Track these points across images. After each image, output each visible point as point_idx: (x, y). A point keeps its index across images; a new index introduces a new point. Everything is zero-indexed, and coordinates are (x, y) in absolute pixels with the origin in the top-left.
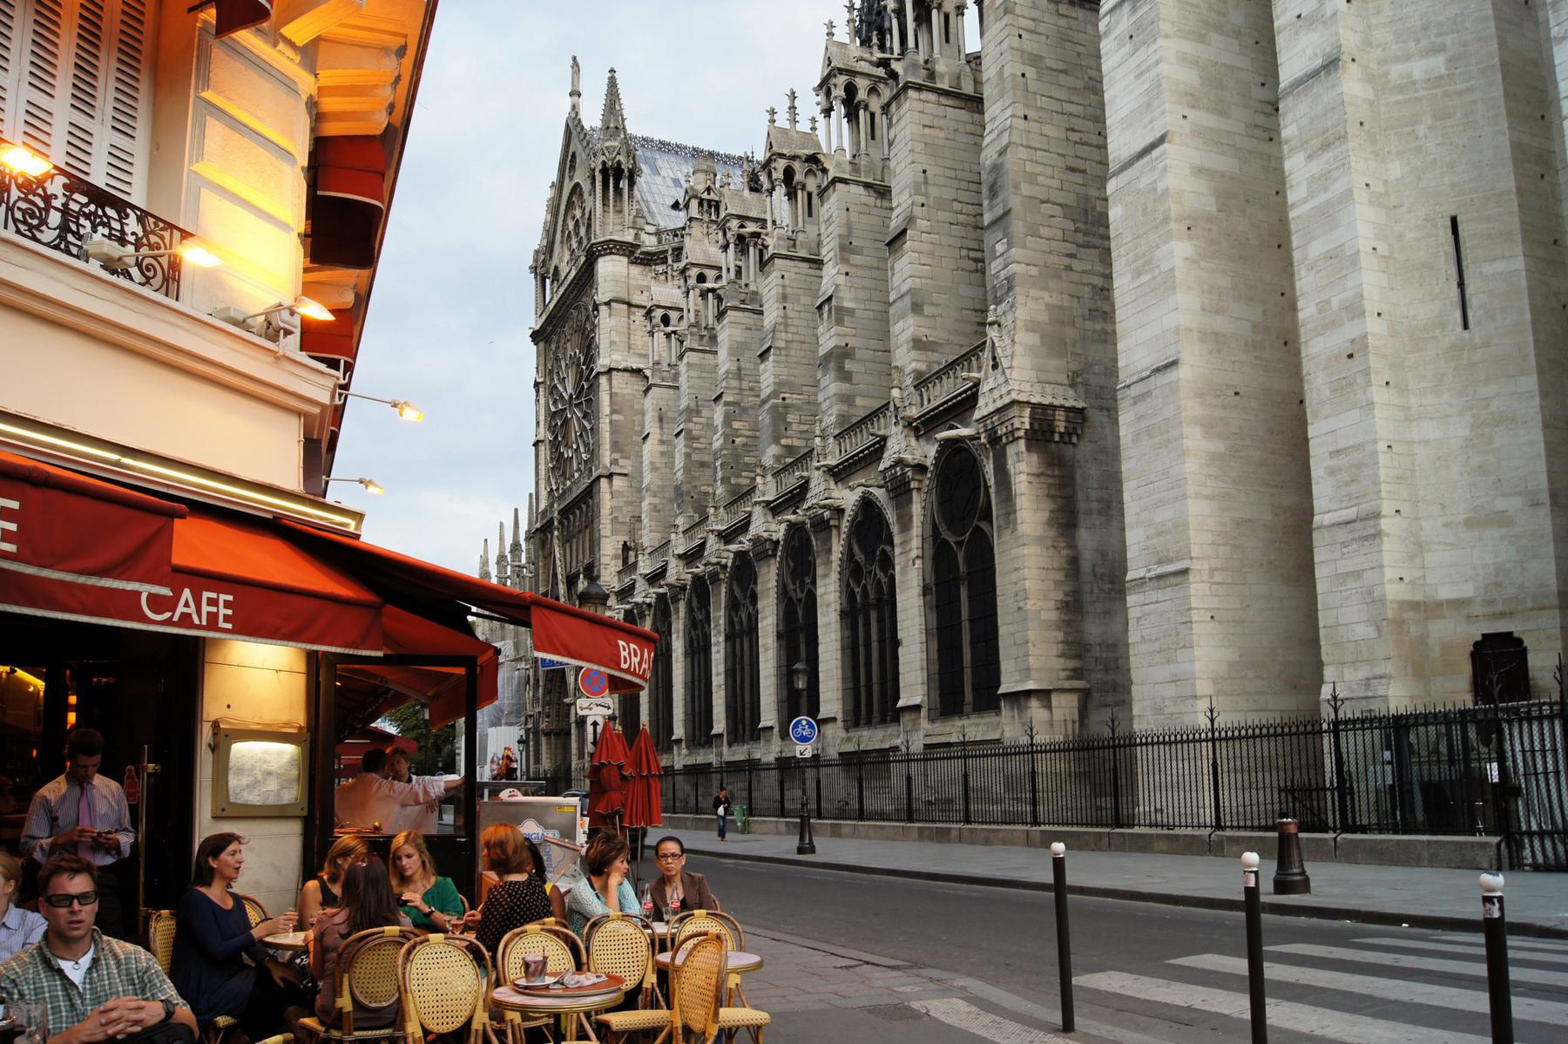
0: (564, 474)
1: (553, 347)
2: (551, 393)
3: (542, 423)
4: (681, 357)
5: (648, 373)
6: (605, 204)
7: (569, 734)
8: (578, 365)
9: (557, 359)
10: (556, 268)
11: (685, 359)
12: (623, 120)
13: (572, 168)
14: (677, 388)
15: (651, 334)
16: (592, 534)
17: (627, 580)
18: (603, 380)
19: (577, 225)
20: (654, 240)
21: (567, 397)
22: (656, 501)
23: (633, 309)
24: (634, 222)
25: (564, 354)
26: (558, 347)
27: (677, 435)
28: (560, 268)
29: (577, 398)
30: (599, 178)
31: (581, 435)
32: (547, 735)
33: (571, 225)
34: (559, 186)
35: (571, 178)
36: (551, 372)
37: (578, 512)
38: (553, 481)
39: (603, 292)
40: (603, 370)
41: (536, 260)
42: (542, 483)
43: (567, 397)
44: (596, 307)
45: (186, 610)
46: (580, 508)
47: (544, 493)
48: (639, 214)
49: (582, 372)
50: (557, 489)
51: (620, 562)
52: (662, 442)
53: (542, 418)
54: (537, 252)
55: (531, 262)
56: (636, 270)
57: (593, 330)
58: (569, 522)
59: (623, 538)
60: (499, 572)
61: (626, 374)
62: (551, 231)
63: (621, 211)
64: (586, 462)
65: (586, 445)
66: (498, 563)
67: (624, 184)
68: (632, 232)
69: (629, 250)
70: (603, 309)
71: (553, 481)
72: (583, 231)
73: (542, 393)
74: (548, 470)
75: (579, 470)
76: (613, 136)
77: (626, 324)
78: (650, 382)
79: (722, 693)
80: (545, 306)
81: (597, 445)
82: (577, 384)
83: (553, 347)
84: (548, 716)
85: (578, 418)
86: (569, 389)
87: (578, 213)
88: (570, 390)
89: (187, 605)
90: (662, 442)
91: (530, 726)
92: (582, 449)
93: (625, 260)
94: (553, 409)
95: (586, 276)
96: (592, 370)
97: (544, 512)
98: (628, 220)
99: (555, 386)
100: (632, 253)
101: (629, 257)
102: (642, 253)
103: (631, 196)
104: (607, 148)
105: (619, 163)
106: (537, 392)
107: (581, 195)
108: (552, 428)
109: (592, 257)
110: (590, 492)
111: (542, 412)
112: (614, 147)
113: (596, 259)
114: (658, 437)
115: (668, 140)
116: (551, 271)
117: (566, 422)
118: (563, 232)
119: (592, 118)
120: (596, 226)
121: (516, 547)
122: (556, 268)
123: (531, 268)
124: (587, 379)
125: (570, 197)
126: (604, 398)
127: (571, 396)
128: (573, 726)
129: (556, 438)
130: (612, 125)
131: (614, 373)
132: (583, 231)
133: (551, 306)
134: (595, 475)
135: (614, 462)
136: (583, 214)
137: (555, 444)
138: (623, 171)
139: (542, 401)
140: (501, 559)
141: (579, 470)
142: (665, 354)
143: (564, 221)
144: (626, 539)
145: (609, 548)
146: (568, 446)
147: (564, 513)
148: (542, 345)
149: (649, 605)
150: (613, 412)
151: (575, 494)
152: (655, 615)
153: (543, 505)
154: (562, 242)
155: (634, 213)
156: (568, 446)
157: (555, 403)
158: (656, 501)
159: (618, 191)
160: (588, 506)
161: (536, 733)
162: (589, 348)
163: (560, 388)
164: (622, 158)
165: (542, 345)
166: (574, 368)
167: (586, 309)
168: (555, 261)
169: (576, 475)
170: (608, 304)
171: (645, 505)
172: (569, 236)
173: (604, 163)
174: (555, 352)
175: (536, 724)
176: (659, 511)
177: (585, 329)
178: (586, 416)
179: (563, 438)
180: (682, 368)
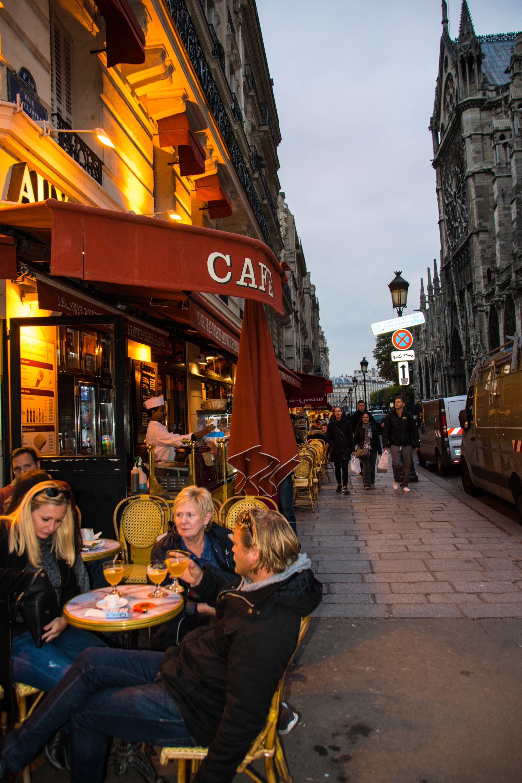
0: (454, 237)
1: (444, 168)
2: (445, 194)
3: (442, 212)
4: (511, 157)
5: (494, 170)
6: (464, 80)
7: (465, 376)
8: (457, 175)
9: (447, 175)
10: (443, 124)
11: (514, 157)
12: (472, 27)
13: (446, 66)
14: (510, 176)
15: (495, 147)
16: (470, 266)
17: (490, 289)
18: (471, 181)
19: (451, 98)
20: (494, 93)
21: (453, 194)
22: (503, 243)
23: (485, 137)
24: (482, 86)
25: (450, 171)
26: (446, 168)
27: (512, 203)
28: (444, 124)
29: (458, 193)
30: (459, 65)
31: (462, 214)
32: (454, 377)
33: (448, 98)
34: (439, 80)
35: (446, 71)
36: (444, 182)
37: (463, 256)
38: (449, 241)
39: (467, 130)
40: (470, 174)
41: (431, 123)
42: (445, 243)
43: (453, 194)
44: (463, 140)
45: (248, 276)
46: (464, 254)
47: (446, 249)
48: (485, 81)
49: (459, 178)
50: (452, 245)
51: (486, 280)
52: (505, 209)
53: (442, 208)
54: (432, 119)
55: (429, 125)
56: (484, 114)
57: (463, 154)
58: (459, 262)
59: (487, 267)
60: (429, 293)
61: (483, 175)
62: (438, 105)
63: (474, 82)
64: (465, 227)
65: (465, 218)
66: (428, 289)
67: (475, 67)
68: (481, 93)
69: (479, 104)
70: (468, 141)
71: (449, 241)
72: (454, 101)
73: (440, 195)
74: (446, 236)
75: (462, 232)
76: (466, 39)
77: (481, 146)
78: (496, 175)
79: (154, 11)
80: (439, 146)
81: (471, 216)
82: (458, 185)
83: (444, 168)
84: (454, 367)
85: (459, 205)
86: (453, 190)
87: (451, 91)
88: (454, 190)
89: (248, 272)
90: (505, 209)
91: (446, 373)
92: (463, 221)
93: (478, 109)
94: (447, 202)
95: (457, 124)
96: (464, 175)
97: (446, 259)
98: (478, 86)
99: (447, 190)
100: (482, 104)
101: (480, 107)
102: (488, 103)
103: (479, 71)
104: (464, 47)
105: (471, 54)
106: (438, 194)
107: (452, 80)
108: (447, 213)
109: (459, 111)
110: (467, 244)
111: (442, 204)
112: (467, 45)
113: (461, 113)
114: (502, 206)
115: (502, 33)
116: (440, 127)
117: (454, 208)
118: (444, 103)
119: (454, 34)
120: (460, 95)
121: (436, 280)
122: (443, 124)
123: (429, 128)
124: (462, 182)
125: (446, 83)
126: (472, 191)
127: (455, 193)
128: (467, 372)
129: (449, 218)
130: (465, 32)
131: (476, 175)
132: (454, 101)
133: (441, 146)
134: (469, 233)
135: (480, 225)
136: (454, 90)
137: (449, 221)
138: (473, 57)
139: (441, 199)
140: (430, 288)
141: (462, 232)
142: (504, 159)
143: (445, 97)
144: (489, 266)
145: (480, 272)
146: (456, 221)
147: (455, 257)
148: (438, 168)
149: (503, 302)
150: (477, 197)
151: (460, 247)
152: (506, 307)
153: (445, 255)
154: (444, 109)
155: (482, 81)
156: (456, 221)
157: (447, 199)
158: (503, 243)
159: (471, 71)
160: (468, 252)
161: (449, 377)
162: (462, 164)
163: (450, 190)
164: (472, 50)
165: (438, 168)
166: (456, 177)
167: (459, 143)
168: (442, 120)
169: (461, 235)
170: (470, 137)
171: (497, 246)
172: (448, 106)
173: (462, 56)
174: (446, 171)
175: (449, 373)
176: (505, 248)
177: (459, 154)
178: (463, 202)
179: (453, 216)
180: (513, 163)
